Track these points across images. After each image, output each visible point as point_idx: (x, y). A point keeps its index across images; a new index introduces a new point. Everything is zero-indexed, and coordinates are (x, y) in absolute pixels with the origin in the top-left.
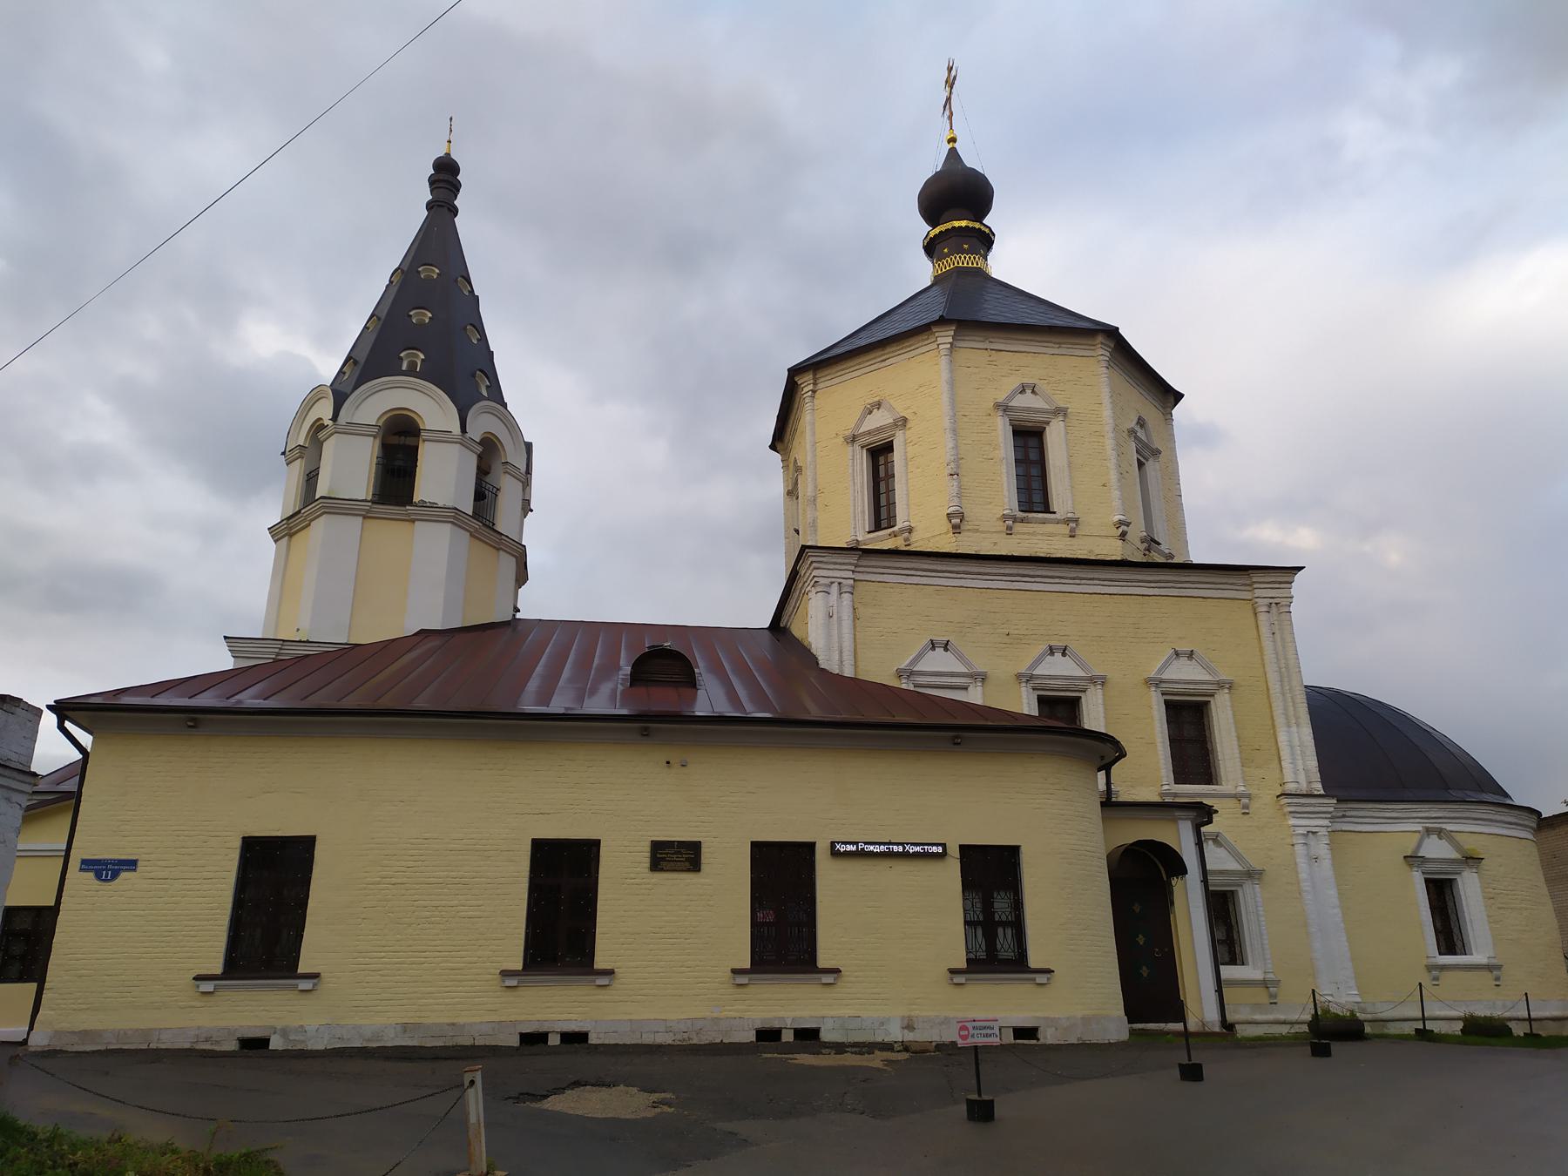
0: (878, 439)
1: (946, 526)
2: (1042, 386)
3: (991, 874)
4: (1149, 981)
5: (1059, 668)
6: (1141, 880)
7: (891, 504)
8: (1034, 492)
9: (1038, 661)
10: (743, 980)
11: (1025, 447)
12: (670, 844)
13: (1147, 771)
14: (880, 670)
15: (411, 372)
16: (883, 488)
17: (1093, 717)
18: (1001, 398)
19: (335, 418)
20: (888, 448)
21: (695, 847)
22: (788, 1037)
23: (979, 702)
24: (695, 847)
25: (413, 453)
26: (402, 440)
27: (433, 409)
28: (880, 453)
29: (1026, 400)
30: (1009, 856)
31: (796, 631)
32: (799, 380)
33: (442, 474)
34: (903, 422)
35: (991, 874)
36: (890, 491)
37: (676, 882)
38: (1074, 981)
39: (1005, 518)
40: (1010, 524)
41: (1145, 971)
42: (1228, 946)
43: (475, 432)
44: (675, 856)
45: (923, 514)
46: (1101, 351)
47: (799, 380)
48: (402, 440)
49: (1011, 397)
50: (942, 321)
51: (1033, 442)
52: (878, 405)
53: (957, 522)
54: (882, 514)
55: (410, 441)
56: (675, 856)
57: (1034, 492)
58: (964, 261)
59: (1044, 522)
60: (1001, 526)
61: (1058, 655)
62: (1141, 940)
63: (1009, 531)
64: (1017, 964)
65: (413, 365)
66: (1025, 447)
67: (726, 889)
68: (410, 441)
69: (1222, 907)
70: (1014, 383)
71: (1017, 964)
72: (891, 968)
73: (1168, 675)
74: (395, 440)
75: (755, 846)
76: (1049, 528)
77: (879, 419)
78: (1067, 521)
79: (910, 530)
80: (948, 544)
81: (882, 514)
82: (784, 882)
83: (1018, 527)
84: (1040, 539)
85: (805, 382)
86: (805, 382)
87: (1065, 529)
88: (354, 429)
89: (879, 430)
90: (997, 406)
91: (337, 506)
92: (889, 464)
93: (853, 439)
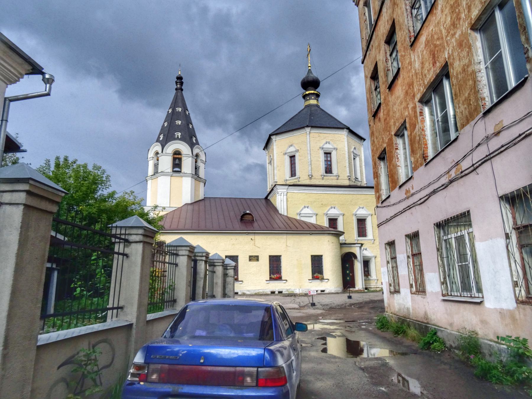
0: (292, 154)
1: (308, 178)
2: (331, 142)
3: (317, 263)
4: (348, 282)
5: (333, 212)
6: (347, 260)
7: (295, 170)
8: (328, 170)
9: (329, 210)
10: (310, 281)
11: (327, 157)
12: (252, 256)
13: (351, 235)
14: (293, 214)
15: (178, 138)
16: (293, 166)
17: (340, 227)
18: (325, 212)
19: (162, 152)
20: (294, 156)
21: (257, 257)
22: (277, 293)
23: (315, 223)
24: (257, 257)
25: (180, 159)
26: (177, 156)
27: (184, 148)
28: (292, 158)
29: (327, 146)
30: (250, 257)
31: (272, 201)
32: (272, 137)
33: (187, 165)
34: (297, 151)
35: (317, 263)
36: (295, 167)
37: (254, 263)
38: (331, 281)
39: (322, 175)
40: (323, 177)
41: (348, 278)
42: (367, 273)
43: (195, 153)
44: (254, 258)
45: (302, 176)
46: (345, 132)
47: (272, 137)
48: (177, 156)
49: (324, 145)
50: (307, 126)
51: (329, 155)
52: (292, 145)
53: (311, 177)
54: (293, 173)
55: (179, 156)
56: (254, 258)
57: (328, 170)
58: (313, 102)
59: (331, 176)
60: (321, 177)
61: (333, 209)
62: (348, 272)
63: (323, 179)
64: (280, 278)
65: (178, 136)
66: (327, 157)
67: (264, 264)
68: (179, 156)
69: (366, 263)
70: (324, 141)
71: (280, 278)
72: (297, 279)
73: (358, 213)
74: (176, 156)
75: (270, 256)
76: (332, 178)
77: (292, 149)
78: (336, 176)
79: (300, 178)
80: (308, 182)
81: (293, 173)
82: (275, 264)
83: (325, 178)
84: (330, 180)
85: (273, 137)
86: (273, 137)
87: (335, 178)
88: (167, 154)
89: (292, 152)
90: (320, 148)
91: (163, 173)
92: (295, 160)
93: (286, 154)
